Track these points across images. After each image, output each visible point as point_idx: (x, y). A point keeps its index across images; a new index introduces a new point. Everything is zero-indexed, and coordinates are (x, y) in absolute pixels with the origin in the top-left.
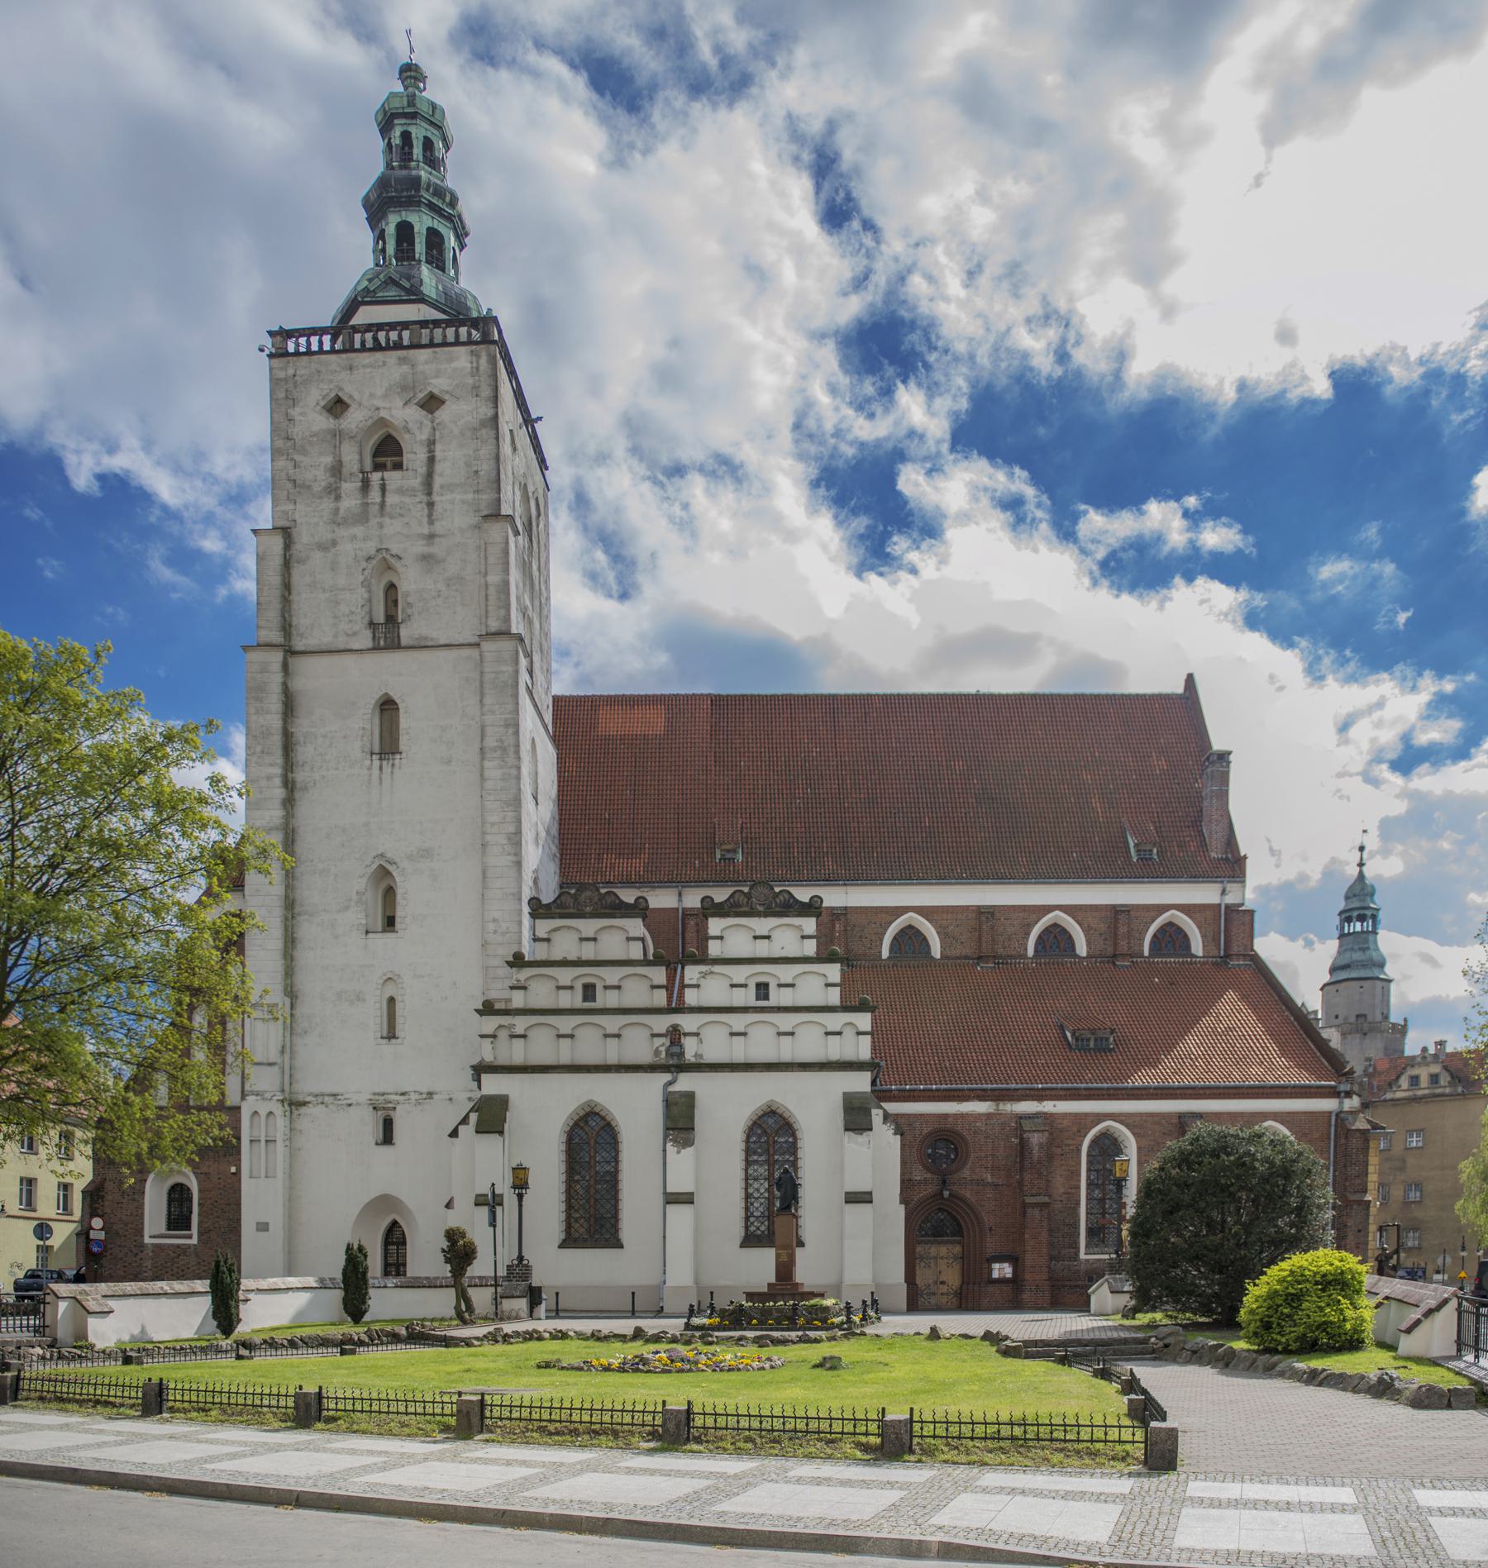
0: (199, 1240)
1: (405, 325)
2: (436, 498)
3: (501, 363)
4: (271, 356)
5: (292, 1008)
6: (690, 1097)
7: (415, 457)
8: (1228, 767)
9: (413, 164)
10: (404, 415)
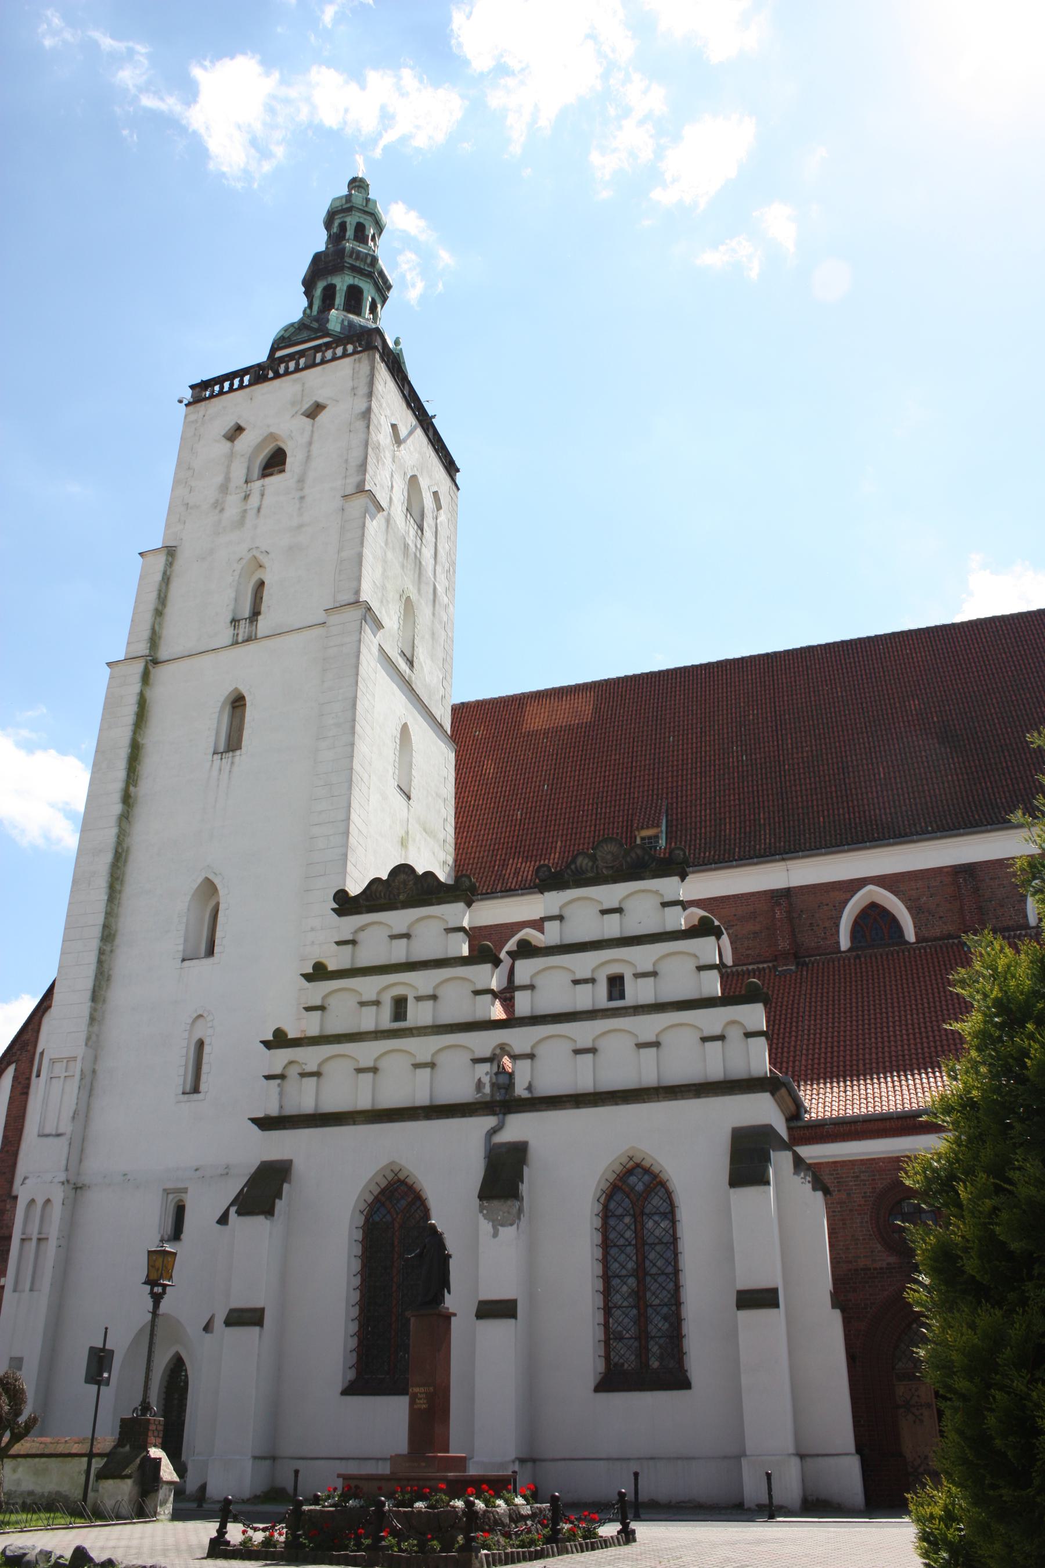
4: (186, 405)
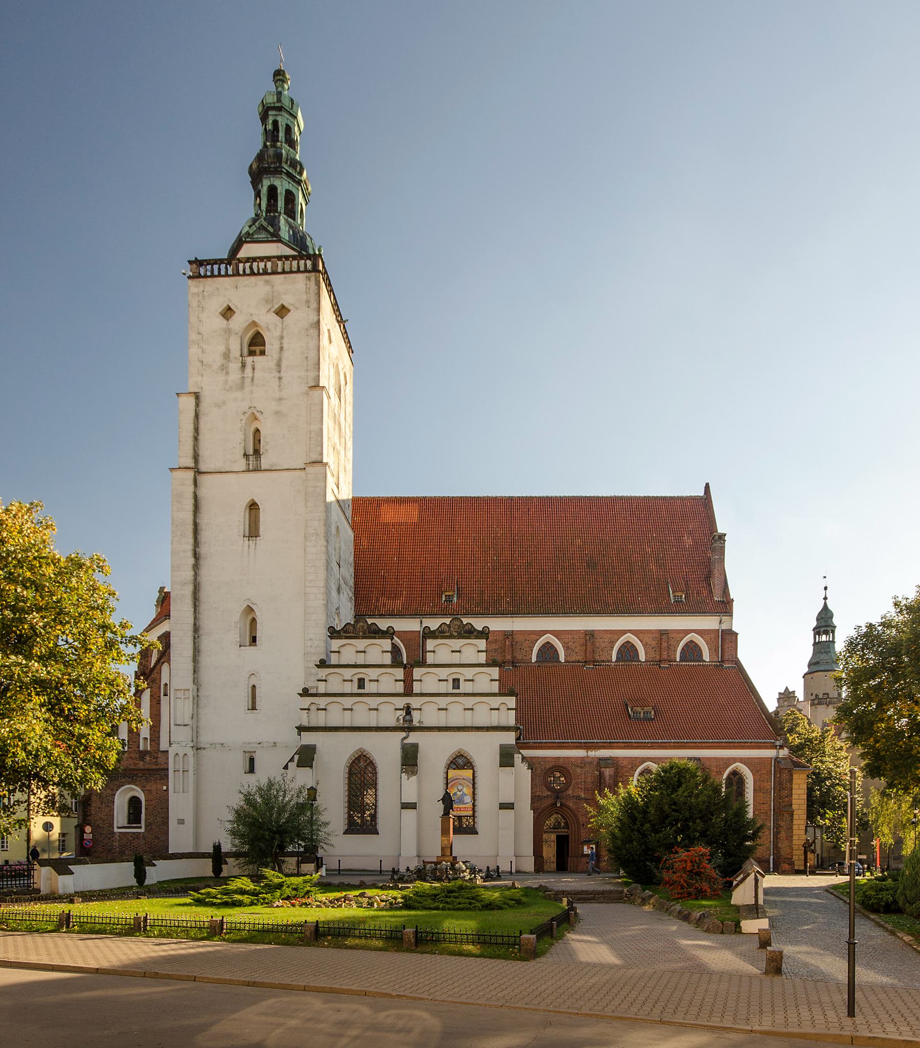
0: (146, 829)
1: (269, 258)
2: (283, 374)
3: (323, 285)
5: (198, 692)
6: (415, 747)
7: (271, 346)
8: (724, 543)
9: (279, 144)
10: (267, 321)
